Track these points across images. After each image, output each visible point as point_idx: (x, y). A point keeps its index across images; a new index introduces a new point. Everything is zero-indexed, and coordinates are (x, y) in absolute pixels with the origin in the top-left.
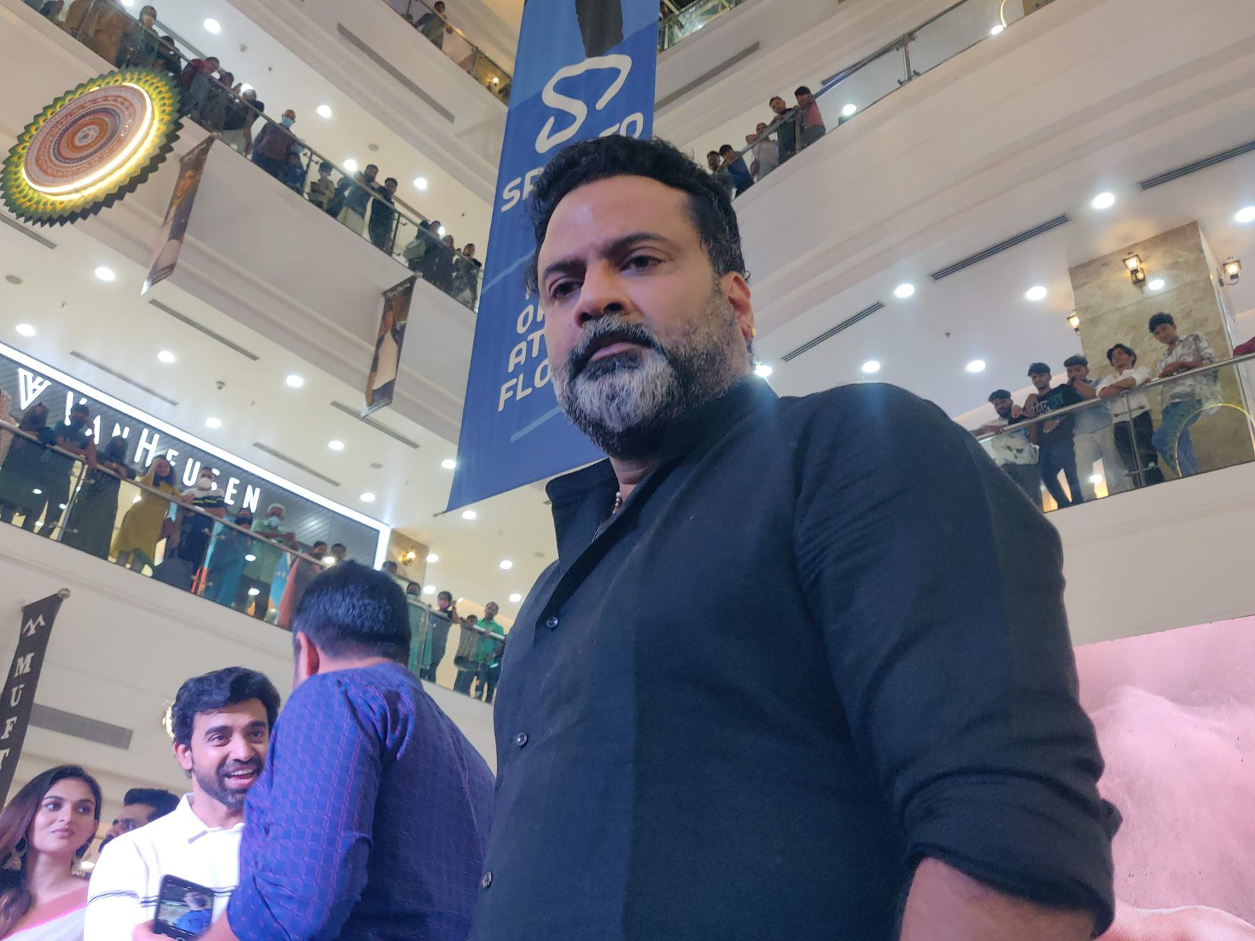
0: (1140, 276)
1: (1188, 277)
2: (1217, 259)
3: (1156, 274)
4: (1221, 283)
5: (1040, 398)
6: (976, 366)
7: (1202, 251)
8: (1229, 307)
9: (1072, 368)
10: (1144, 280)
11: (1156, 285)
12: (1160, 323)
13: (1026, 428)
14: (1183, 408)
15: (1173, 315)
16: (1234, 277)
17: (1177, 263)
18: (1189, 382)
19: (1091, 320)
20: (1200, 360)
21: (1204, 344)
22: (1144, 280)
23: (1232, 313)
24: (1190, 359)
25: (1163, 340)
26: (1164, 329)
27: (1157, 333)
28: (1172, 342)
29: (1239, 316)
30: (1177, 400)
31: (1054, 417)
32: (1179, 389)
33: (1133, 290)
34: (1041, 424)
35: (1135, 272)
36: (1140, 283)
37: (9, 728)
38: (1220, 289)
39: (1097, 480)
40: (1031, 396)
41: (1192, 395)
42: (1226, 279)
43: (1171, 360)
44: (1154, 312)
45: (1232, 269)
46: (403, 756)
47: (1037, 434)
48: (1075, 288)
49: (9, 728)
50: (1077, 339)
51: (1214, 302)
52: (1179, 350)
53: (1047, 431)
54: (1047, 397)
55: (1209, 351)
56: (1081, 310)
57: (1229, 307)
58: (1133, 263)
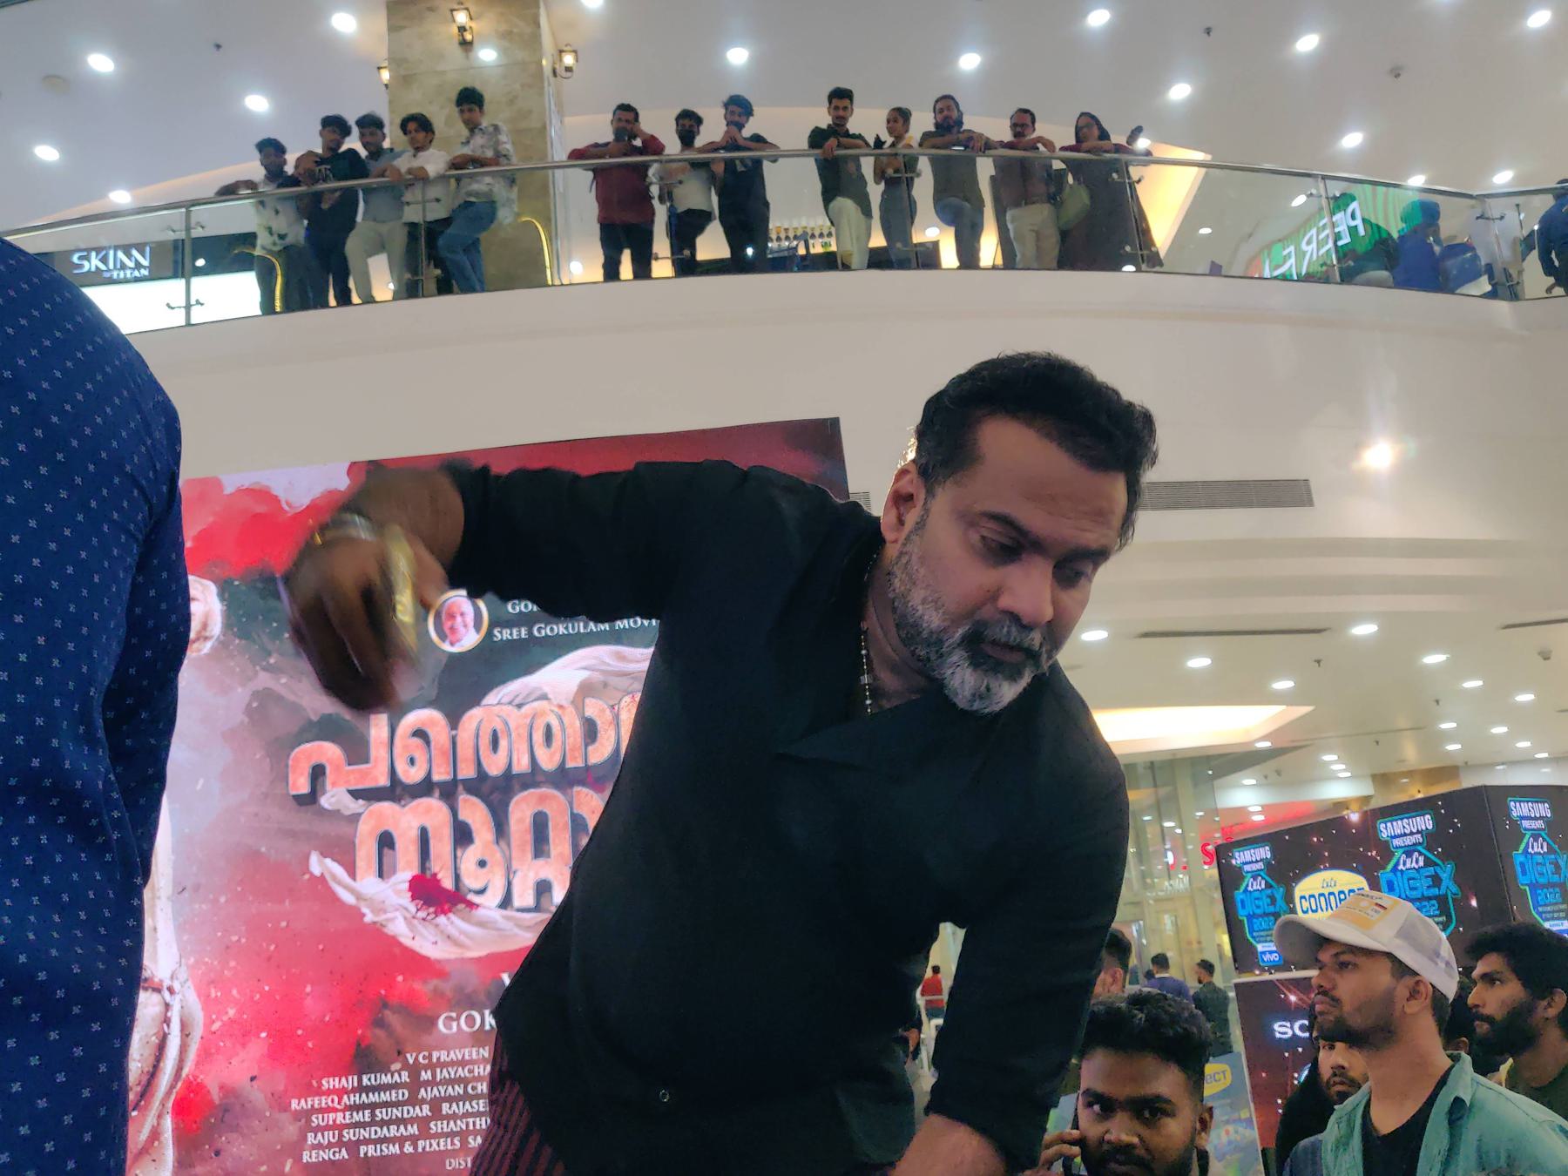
0: (468, 37)
1: (521, 55)
2: (556, 44)
3: (486, 42)
4: (555, 73)
5: (321, 160)
6: (257, 103)
7: (538, 25)
8: (559, 105)
9: (367, 131)
10: (471, 43)
11: (487, 55)
12: (470, 99)
13: (298, 198)
14: (479, 214)
15: (487, 97)
16: (569, 69)
17: (511, 32)
18: (488, 179)
19: (405, 79)
20: (499, 157)
21: (503, 138)
22: (471, 43)
23: (561, 113)
24: (489, 154)
25: (467, 122)
26: (470, 110)
27: (462, 111)
28: (473, 127)
29: (567, 120)
30: (473, 199)
31: (334, 190)
32: (475, 187)
33: (457, 51)
34: (318, 197)
35: (462, 29)
36: (466, 45)
37: (1124, 1168)
38: (552, 79)
39: (384, 286)
40: (310, 153)
41: (489, 194)
42: (561, 71)
43: (467, 151)
44: (469, 83)
45: (569, 60)
46: (1305, 1148)
47: (311, 208)
48: (393, 29)
49: (1124, 1168)
50: (384, 98)
51: (541, 94)
52: (479, 140)
53: (325, 206)
54: (336, 162)
55: (508, 146)
56: (395, 62)
57: (559, 105)
58: (461, 18)
